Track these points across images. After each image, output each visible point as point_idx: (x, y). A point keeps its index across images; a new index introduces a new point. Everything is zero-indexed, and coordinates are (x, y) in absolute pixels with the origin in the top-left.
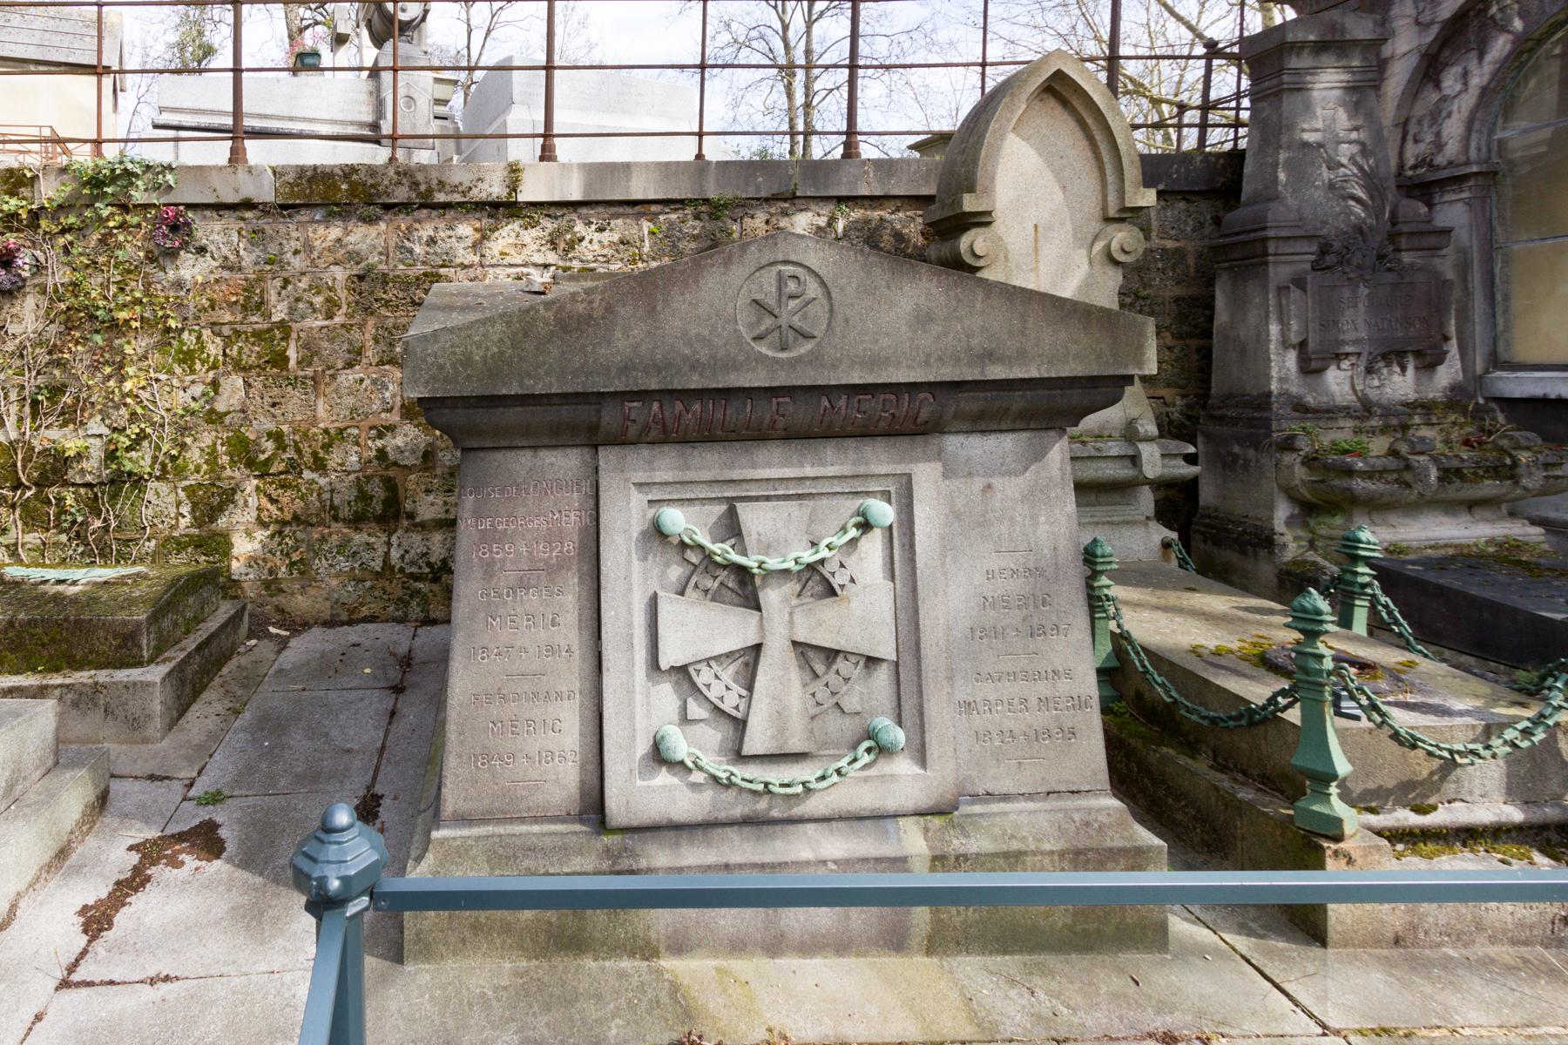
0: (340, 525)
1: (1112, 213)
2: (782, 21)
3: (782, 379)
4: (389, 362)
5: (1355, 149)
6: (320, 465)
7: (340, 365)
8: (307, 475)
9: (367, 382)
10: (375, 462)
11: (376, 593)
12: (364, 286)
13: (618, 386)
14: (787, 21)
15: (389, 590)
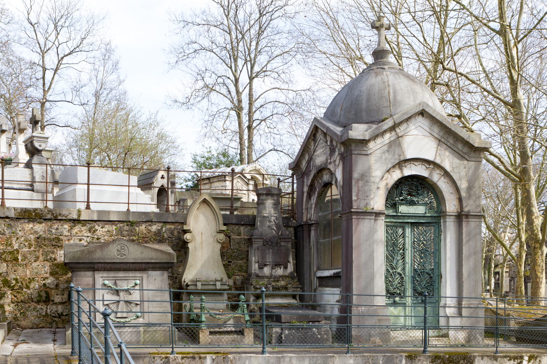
0: (34, 303)
1: (218, 231)
2: (235, 76)
3: (121, 261)
4: (46, 261)
5: (275, 218)
6: (28, 287)
7: (33, 261)
8: (24, 290)
9: (40, 266)
10: (43, 287)
11: (44, 321)
12: (39, 240)
13: (97, 261)
14: (237, 77)
15: (47, 320)
